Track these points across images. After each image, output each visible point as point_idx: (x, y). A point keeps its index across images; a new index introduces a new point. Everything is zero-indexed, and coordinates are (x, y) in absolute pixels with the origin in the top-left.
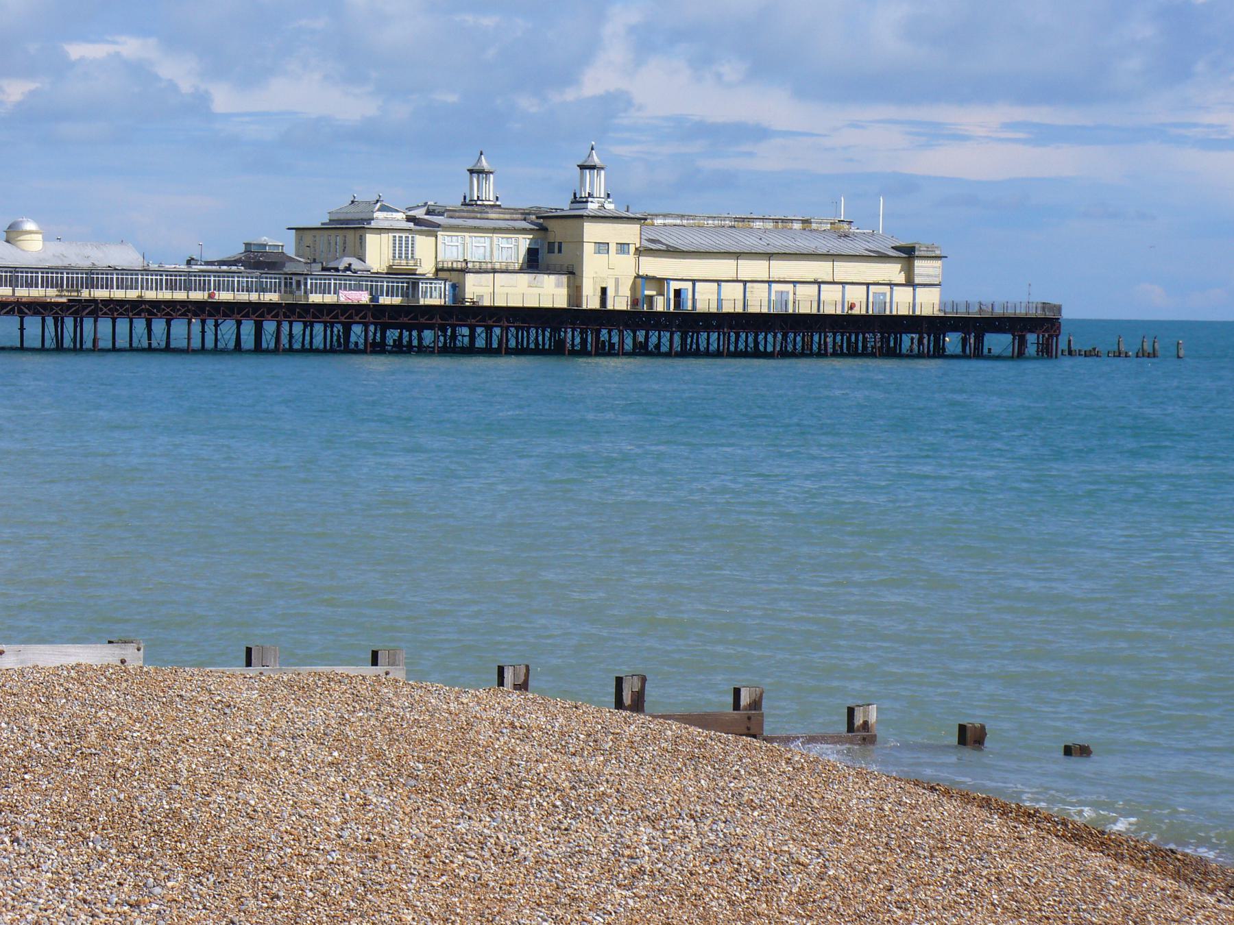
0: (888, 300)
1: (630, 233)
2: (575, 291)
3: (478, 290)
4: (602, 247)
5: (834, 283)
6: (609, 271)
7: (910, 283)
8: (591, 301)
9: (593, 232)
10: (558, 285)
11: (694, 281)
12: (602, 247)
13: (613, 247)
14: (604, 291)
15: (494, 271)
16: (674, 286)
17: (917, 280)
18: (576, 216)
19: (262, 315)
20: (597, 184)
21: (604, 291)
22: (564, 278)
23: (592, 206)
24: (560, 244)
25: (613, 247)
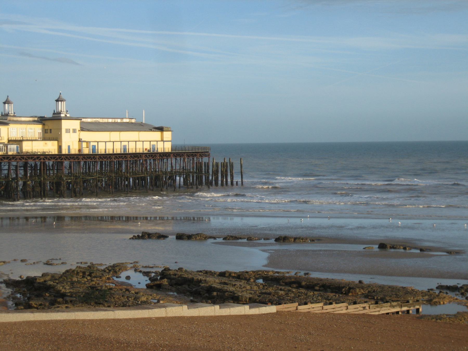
0: (97, 148)
1: (76, 124)
2: (60, 148)
3: (27, 147)
4: (68, 131)
5: (139, 141)
6: (72, 139)
7: (162, 140)
8: (65, 151)
9: (65, 124)
10: (53, 145)
11: (98, 142)
12: (68, 131)
13: (71, 131)
14: (69, 147)
15: (32, 140)
16: (92, 144)
17: (164, 140)
18: (57, 117)
19: (10, 160)
20: (62, 107)
21: (69, 147)
22: (56, 142)
23: (62, 115)
24: (51, 130)
25: (71, 131)
